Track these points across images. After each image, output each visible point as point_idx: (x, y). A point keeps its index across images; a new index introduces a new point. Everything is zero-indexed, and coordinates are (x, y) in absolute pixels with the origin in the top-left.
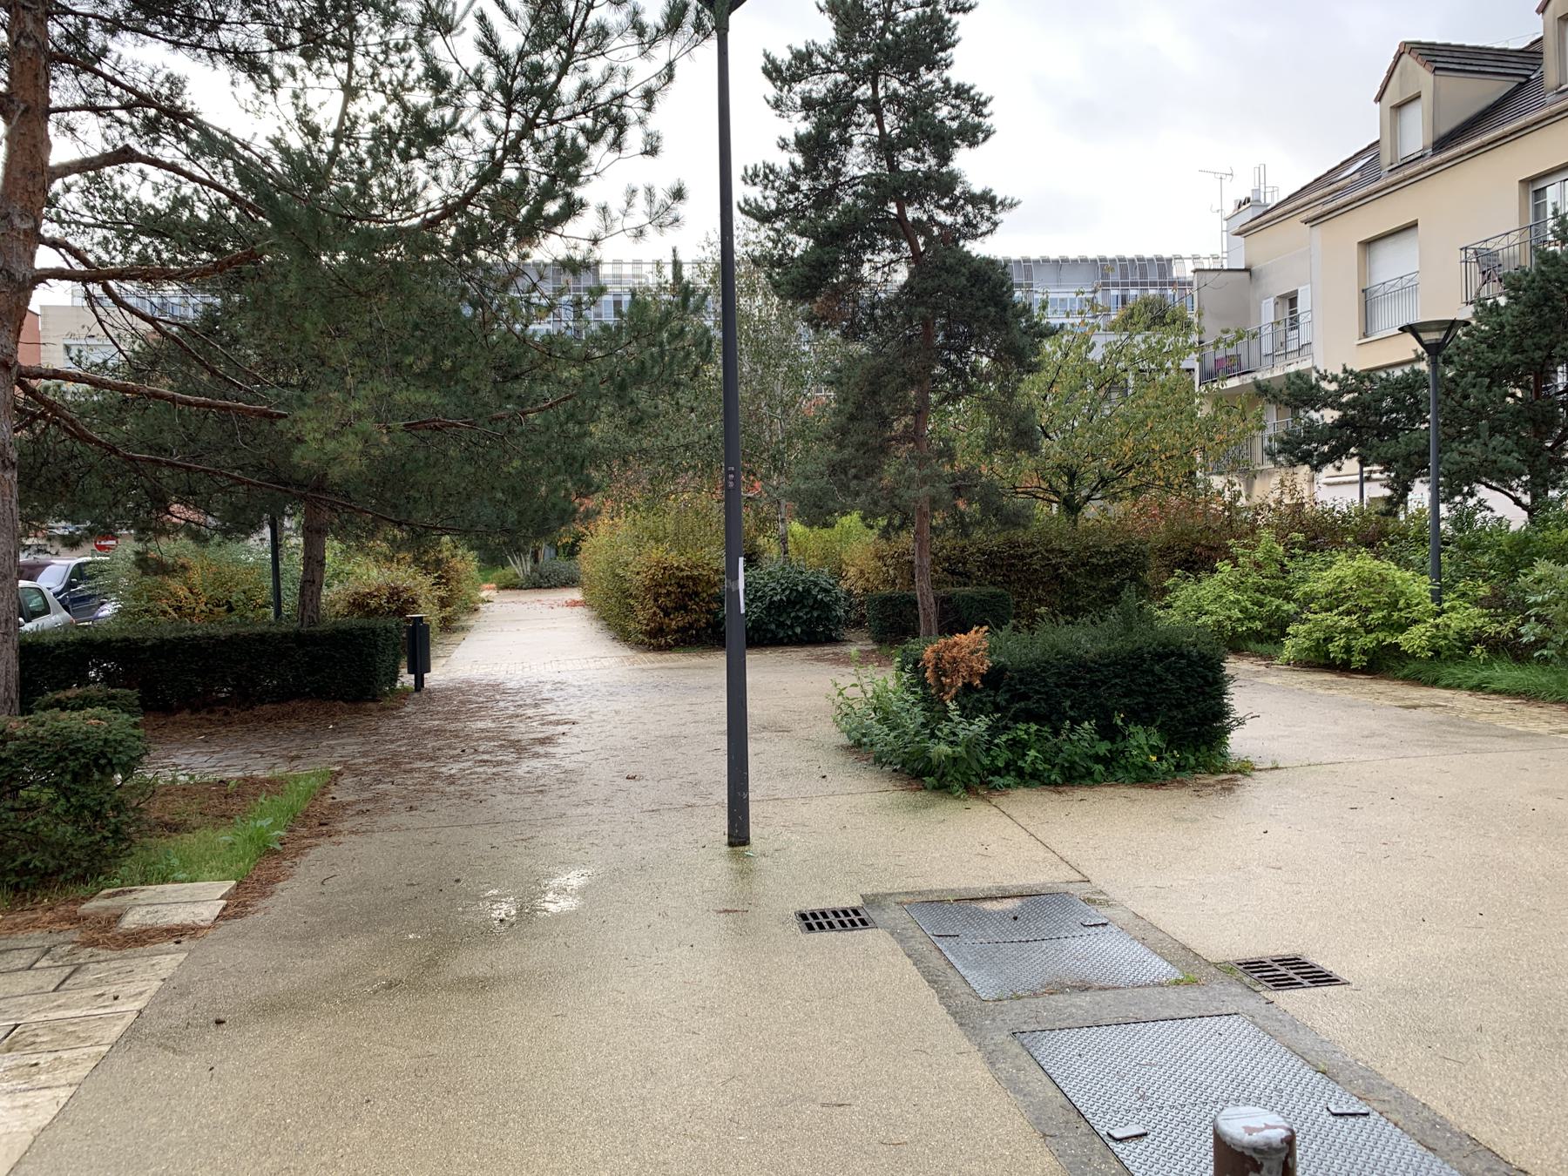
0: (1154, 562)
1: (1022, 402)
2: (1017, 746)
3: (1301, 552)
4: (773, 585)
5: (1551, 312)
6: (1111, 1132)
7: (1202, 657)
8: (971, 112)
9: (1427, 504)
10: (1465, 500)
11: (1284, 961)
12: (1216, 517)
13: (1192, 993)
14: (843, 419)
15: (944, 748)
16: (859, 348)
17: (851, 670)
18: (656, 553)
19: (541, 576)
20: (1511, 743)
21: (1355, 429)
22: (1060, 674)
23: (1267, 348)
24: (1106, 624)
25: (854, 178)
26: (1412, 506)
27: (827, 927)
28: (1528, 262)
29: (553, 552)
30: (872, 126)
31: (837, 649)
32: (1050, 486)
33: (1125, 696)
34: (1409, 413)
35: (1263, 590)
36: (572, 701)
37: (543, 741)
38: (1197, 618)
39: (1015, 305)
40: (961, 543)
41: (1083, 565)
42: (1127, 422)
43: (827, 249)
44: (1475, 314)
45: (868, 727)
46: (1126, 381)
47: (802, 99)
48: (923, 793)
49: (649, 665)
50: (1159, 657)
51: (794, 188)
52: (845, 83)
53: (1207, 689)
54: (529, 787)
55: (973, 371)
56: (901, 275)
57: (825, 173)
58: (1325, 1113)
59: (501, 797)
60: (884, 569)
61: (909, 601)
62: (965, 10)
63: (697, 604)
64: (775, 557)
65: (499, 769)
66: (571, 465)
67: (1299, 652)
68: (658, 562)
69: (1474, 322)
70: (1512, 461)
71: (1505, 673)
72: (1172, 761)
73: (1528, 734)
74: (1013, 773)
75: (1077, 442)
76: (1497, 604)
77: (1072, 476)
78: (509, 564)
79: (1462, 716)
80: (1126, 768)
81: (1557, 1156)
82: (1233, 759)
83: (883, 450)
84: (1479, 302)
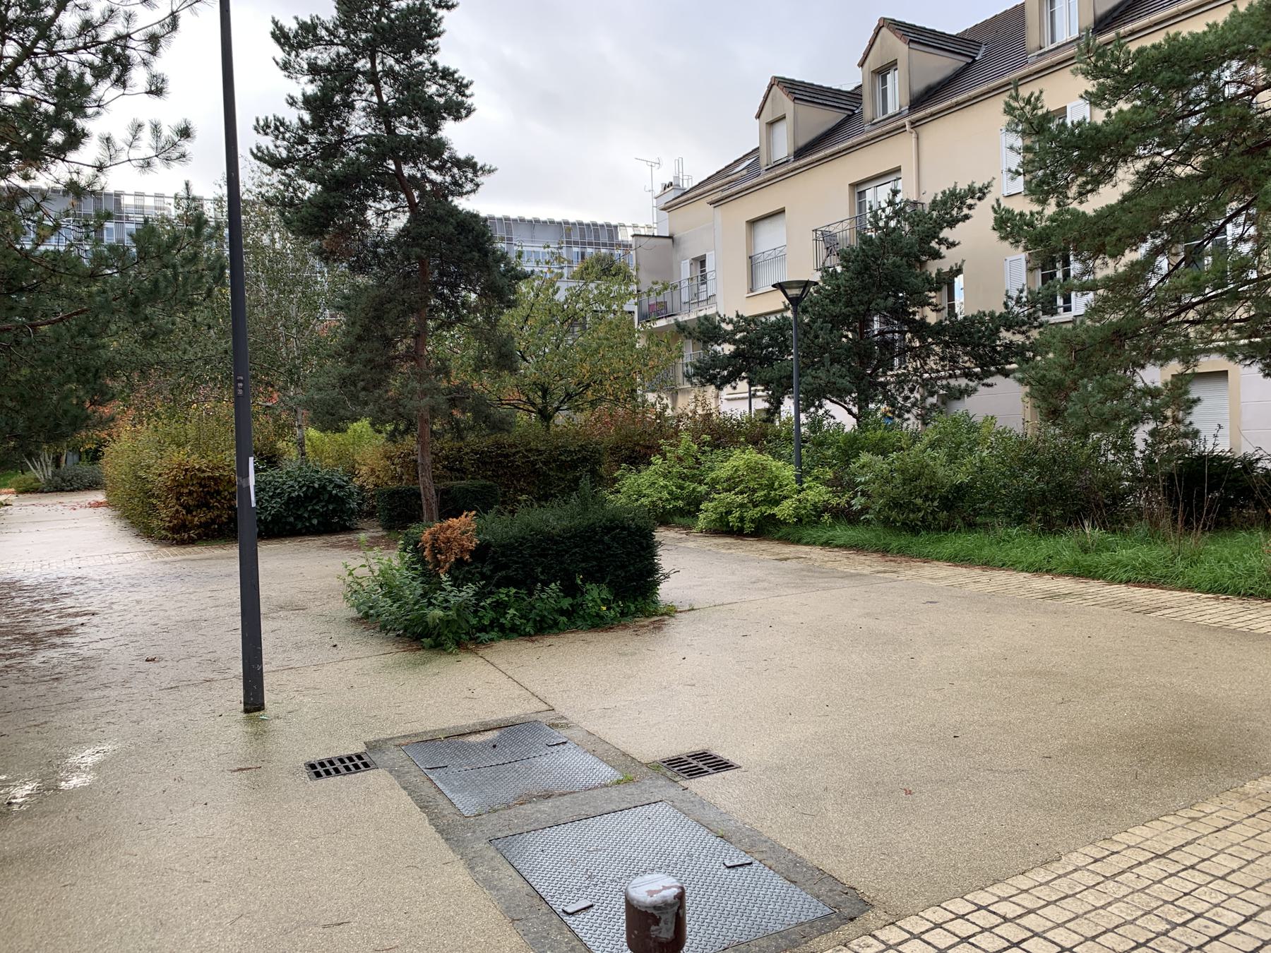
0: (607, 459)
1: (502, 331)
2: (500, 607)
3: (709, 449)
4: (291, 483)
5: (869, 278)
6: (565, 909)
7: (638, 528)
8: (456, 92)
9: (793, 414)
10: (817, 411)
11: (696, 756)
12: (651, 424)
13: (630, 789)
14: (352, 339)
15: (439, 613)
16: (361, 280)
17: (361, 554)
18: (177, 456)
19: (63, 480)
20: (846, 582)
21: (745, 359)
22: (533, 547)
23: (685, 298)
24: (568, 506)
25: (356, 137)
26: (784, 416)
27: (333, 773)
28: (855, 243)
29: (76, 458)
30: (372, 95)
31: (351, 537)
32: (528, 399)
33: (583, 562)
34: (780, 348)
35: (684, 477)
36: (92, 594)
37: (60, 633)
38: (637, 500)
39: (494, 252)
40: (457, 445)
41: (555, 461)
42: (585, 350)
43: (333, 194)
44: (822, 277)
45: (374, 601)
46: (584, 318)
47: (308, 64)
48: (421, 652)
49: (172, 558)
50: (608, 530)
51: (303, 141)
52: (346, 55)
53: (643, 553)
54: (44, 676)
55: (463, 304)
56: (399, 222)
57: (330, 130)
58: (723, 867)
59: (12, 687)
60: (392, 467)
61: (414, 494)
62: (449, 7)
63: (219, 502)
64: (294, 459)
65: (13, 661)
66: (84, 375)
67: (708, 523)
68: (180, 464)
69: (821, 284)
70: (845, 382)
71: (843, 533)
72: (618, 609)
73: (858, 575)
74: (496, 629)
75: (547, 365)
76: (837, 484)
77: (545, 392)
78: (29, 469)
79: (816, 564)
80: (583, 617)
81: (874, 874)
82: (662, 605)
83: (388, 366)
84: (824, 270)
